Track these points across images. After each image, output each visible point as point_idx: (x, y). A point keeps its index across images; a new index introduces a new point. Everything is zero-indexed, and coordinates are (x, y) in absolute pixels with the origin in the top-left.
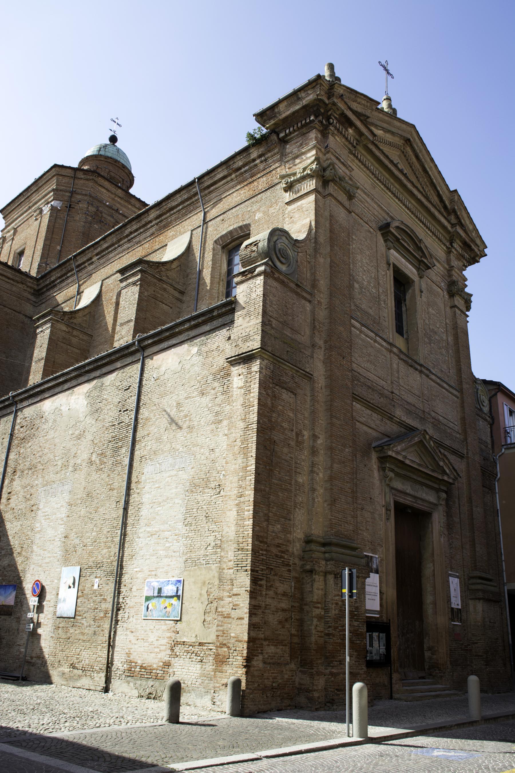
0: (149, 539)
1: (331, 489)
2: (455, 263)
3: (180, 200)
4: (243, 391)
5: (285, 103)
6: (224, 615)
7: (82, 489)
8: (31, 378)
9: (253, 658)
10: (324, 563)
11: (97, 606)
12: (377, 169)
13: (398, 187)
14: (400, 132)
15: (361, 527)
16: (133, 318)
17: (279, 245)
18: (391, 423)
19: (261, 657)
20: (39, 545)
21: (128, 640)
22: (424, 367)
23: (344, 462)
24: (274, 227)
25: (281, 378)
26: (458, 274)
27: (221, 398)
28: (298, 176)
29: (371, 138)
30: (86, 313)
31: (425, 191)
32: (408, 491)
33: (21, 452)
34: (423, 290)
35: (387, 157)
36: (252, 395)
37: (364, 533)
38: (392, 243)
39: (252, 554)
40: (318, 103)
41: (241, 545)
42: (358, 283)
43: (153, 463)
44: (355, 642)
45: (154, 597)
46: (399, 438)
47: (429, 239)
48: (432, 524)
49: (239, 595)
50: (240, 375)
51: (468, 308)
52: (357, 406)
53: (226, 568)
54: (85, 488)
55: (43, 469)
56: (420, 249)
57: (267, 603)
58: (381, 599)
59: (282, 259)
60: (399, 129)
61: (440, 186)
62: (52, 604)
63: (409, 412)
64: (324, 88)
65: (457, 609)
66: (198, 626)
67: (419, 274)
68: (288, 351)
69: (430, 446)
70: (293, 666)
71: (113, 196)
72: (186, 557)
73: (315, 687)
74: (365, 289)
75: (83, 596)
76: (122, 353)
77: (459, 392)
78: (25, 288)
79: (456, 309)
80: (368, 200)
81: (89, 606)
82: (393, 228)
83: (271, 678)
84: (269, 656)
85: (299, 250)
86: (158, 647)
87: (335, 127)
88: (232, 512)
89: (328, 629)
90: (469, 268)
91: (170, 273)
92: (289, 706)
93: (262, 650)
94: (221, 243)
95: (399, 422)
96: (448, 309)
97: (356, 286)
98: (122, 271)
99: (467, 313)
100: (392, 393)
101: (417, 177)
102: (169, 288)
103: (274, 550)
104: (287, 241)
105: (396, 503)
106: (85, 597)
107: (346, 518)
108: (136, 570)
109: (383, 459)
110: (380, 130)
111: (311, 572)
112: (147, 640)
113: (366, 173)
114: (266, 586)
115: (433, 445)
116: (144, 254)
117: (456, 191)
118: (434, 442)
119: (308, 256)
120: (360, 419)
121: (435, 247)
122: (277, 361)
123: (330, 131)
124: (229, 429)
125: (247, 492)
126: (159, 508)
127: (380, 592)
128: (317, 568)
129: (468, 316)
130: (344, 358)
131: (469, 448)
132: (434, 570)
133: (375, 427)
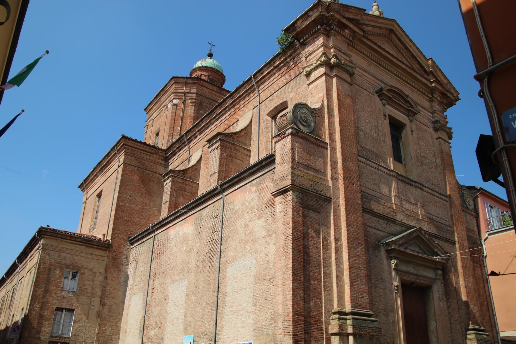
4: (282, 214)
14: (385, 26)
16: (217, 171)
24: (295, 103)
27: (270, 219)
28: (314, 65)
32: (411, 272)
34: (413, 129)
42: (362, 131)
48: (432, 293)
51: (450, 138)
59: (304, 123)
61: (419, 57)
69: (426, 238)
71: (211, 91)
76: (211, 194)
79: (441, 140)
80: (366, 74)
85: (317, 115)
87: (335, 30)
90: (448, 110)
97: (361, 133)
98: (209, 141)
99: (450, 141)
101: (402, 53)
120: (370, 225)
124: (275, 240)
132: (436, 326)
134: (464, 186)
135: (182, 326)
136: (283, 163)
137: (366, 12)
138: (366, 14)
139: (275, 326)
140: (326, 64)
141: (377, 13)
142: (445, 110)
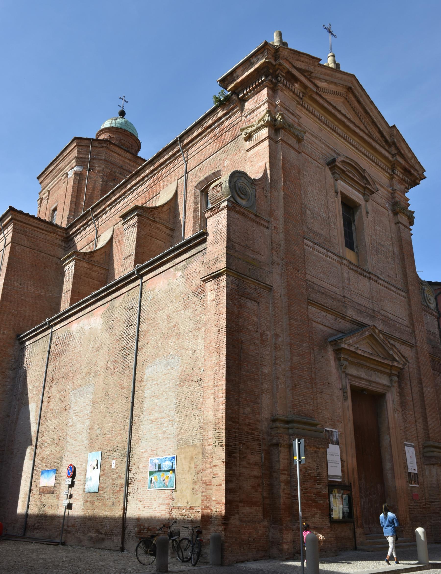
0: (151, 425)
1: (292, 377)
2: (398, 187)
3: (167, 157)
4: (214, 302)
5: (241, 68)
6: (207, 483)
7: (101, 390)
8: (62, 306)
9: (231, 518)
10: (287, 437)
11: (114, 482)
12: (323, 114)
13: (342, 128)
14: (342, 82)
15: (321, 407)
16: (133, 252)
17: (239, 184)
18: (344, 321)
19: (237, 516)
20: (71, 437)
21: (138, 508)
22: (372, 274)
23: (302, 355)
25: (246, 291)
26: (401, 196)
27: (199, 309)
28: (255, 127)
29: (315, 90)
30: (102, 252)
31: (367, 130)
32: (362, 376)
33: (57, 364)
34: (368, 211)
35: (330, 104)
36: (221, 305)
37: (325, 412)
38: (339, 175)
39: (226, 432)
40: (267, 65)
41: (217, 425)
42: (310, 209)
43: (152, 365)
44: (319, 502)
45: (156, 472)
46: (352, 333)
47: (373, 169)
48: (386, 402)
49: (217, 466)
50: (212, 290)
51: (412, 223)
52: (312, 309)
53: (207, 445)
54: (103, 389)
55: (73, 377)
56: (364, 178)
57: (241, 472)
58: (343, 466)
59: (242, 195)
60: (340, 80)
62: (82, 482)
63: (360, 312)
64: (271, 52)
65: (414, 473)
66: (188, 493)
67: (364, 199)
68: (250, 269)
69: (380, 338)
70: (266, 523)
71: (123, 159)
72: (178, 438)
73: (285, 540)
74: (316, 214)
75: (104, 475)
77: (406, 293)
78: (57, 237)
79: (400, 225)
80: (316, 141)
81: (108, 483)
82: (339, 163)
83: (247, 533)
84: (245, 515)
85: (257, 187)
86: (160, 513)
87: (283, 84)
88: (210, 399)
89: (294, 492)
91: (161, 215)
92: (264, 556)
93: (238, 511)
94: (200, 188)
95: (351, 320)
96: (393, 225)
97: (308, 212)
98: (124, 217)
99: (410, 227)
100: (344, 297)
101: (360, 119)
102: (161, 227)
103: (246, 429)
104: (245, 180)
105: (352, 387)
106: (106, 475)
107: (306, 400)
108: (142, 451)
109: (338, 351)
110: (324, 82)
111: (277, 445)
112: (151, 507)
113: (313, 119)
114: (240, 458)
115: (382, 337)
116: (143, 202)
117: (394, 126)
118: (383, 335)
119: (265, 192)
121: (378, 174)
122: (241, 277)
123: (279, 87)
124: (205, 334)
125: (220, 383)
126: (157, 401)
127: (342, 460)
128: (281, 442)
129: (411, 230)
130: (298, 271)
131: (417, 339)
133: (330, 325)
134: (424, 281)
135: (86, 441)
136: (216, 242)
137: (321, 62)
138: (320, 65)
139: (204, 436)
140: (268, 124)
141: (332, 65)
142: (407, 189)
